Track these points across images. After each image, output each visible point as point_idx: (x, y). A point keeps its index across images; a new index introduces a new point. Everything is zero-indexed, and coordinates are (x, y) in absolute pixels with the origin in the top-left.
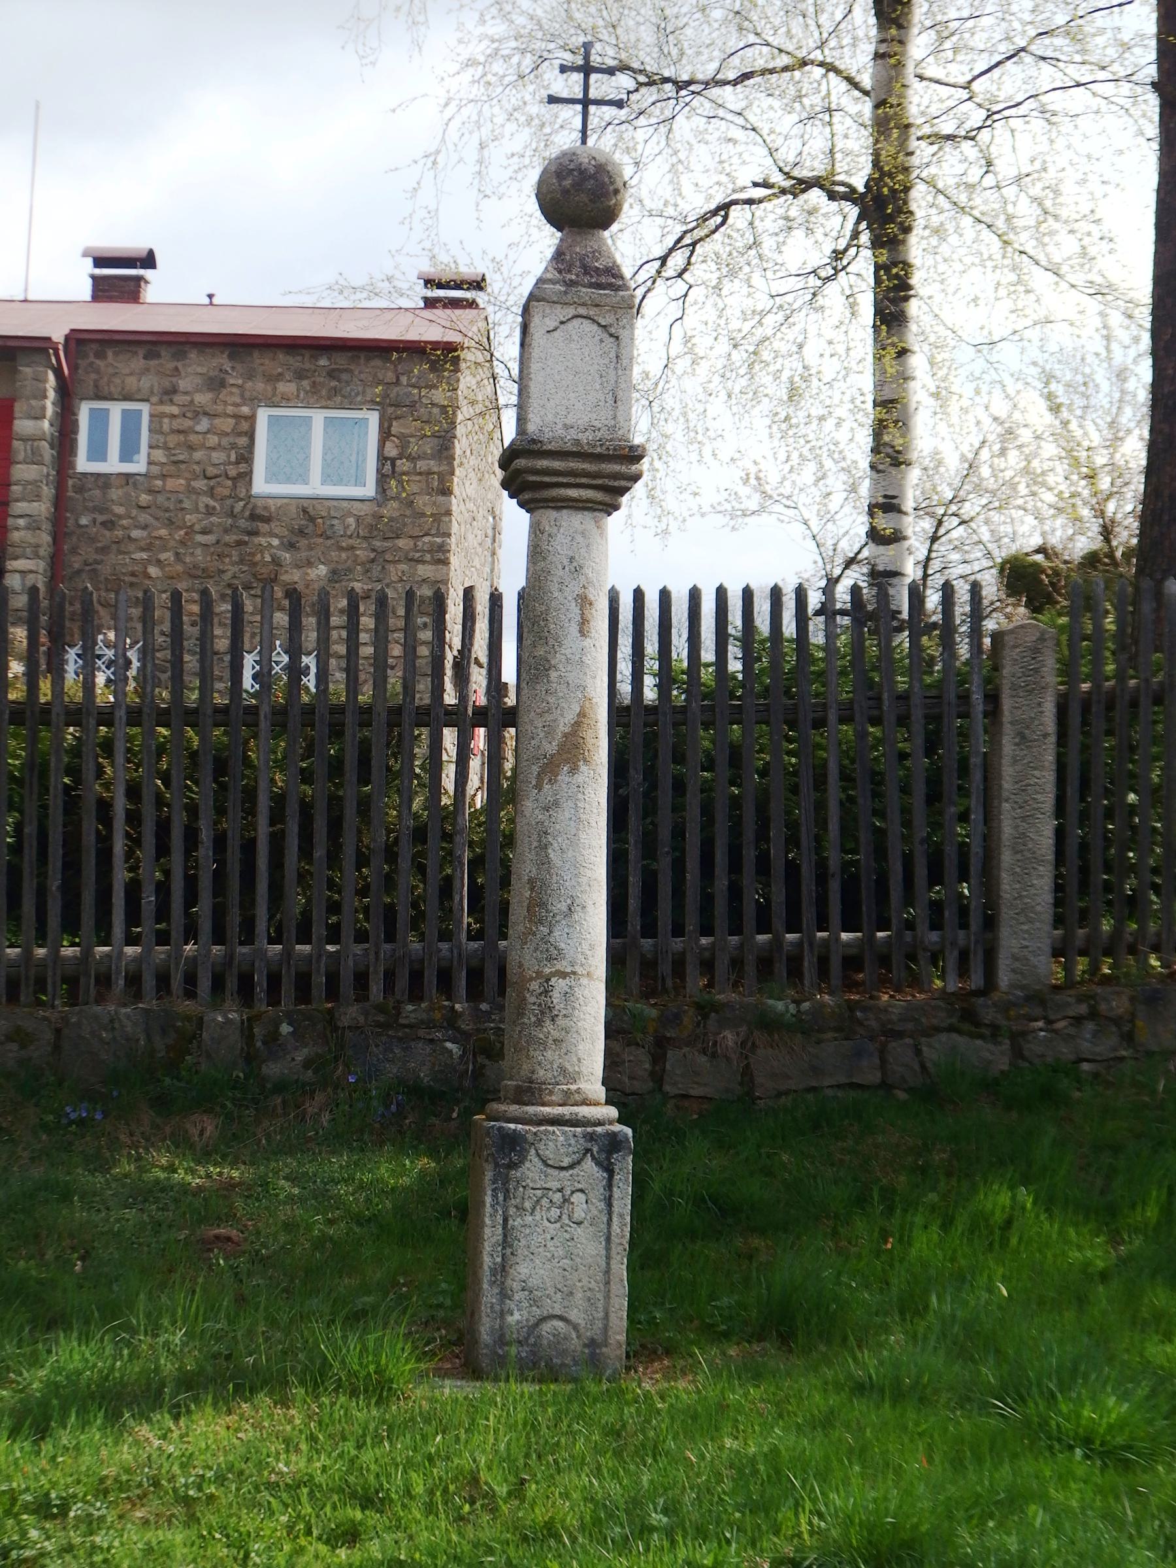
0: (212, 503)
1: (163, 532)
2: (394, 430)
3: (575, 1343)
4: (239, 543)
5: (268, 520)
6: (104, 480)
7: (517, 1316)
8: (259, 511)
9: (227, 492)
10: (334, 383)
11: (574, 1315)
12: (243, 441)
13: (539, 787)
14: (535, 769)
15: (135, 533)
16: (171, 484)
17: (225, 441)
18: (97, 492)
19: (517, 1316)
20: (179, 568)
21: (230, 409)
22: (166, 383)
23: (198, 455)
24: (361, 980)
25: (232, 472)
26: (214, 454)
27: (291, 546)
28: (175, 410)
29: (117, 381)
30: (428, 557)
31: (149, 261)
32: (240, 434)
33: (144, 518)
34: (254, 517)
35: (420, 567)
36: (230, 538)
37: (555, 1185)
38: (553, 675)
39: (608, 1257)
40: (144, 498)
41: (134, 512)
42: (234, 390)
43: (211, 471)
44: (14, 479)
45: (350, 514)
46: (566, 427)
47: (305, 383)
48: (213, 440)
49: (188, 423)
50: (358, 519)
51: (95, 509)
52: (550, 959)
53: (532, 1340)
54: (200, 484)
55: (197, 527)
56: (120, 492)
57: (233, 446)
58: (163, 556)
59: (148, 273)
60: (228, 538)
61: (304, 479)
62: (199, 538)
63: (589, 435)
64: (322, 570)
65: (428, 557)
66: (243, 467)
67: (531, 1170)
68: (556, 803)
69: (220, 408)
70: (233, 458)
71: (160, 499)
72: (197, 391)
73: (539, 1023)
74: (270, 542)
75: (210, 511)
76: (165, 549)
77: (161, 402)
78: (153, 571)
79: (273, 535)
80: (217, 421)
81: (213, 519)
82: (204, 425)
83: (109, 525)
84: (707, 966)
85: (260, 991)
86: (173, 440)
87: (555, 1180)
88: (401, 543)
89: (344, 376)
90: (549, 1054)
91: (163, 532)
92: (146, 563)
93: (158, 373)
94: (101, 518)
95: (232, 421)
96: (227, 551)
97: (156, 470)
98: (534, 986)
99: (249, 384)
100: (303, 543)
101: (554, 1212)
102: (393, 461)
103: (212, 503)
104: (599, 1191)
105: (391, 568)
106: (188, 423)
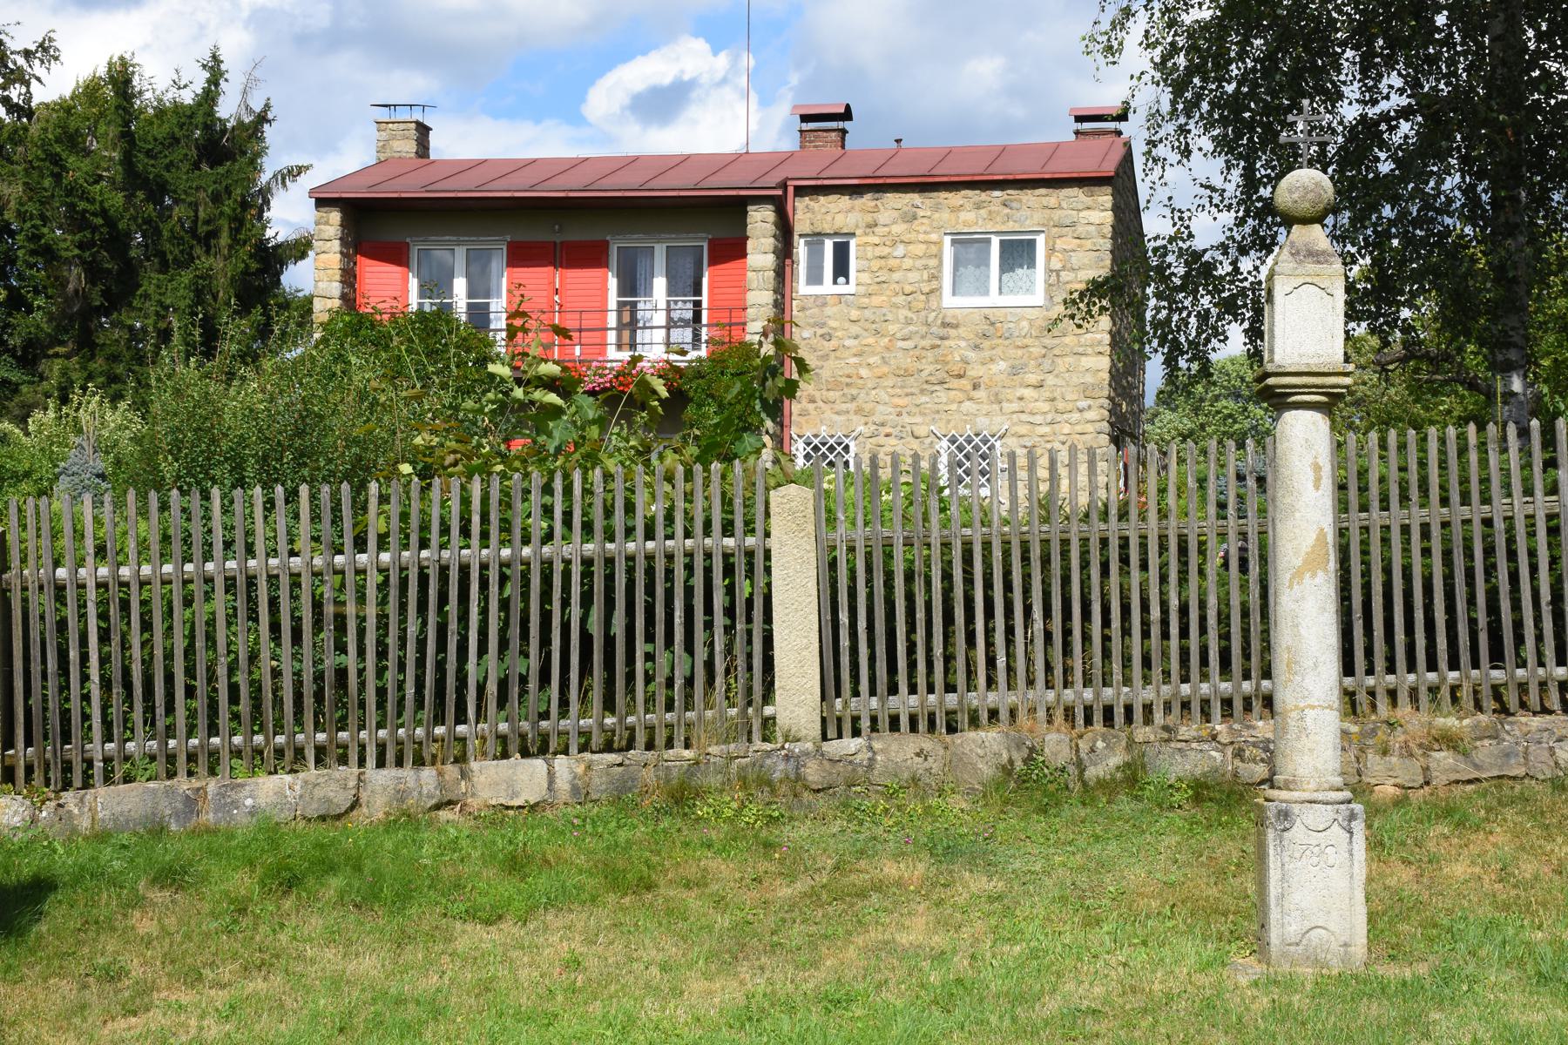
0: (910, 315)
1: (871, 340)
2: (1058, 247)
3: (1334, 946)
4: (934, 347)
5: (956, 326)
6: (822, 301)
7: (1294, 927)
8: (948, 320)
9: (921, 306)
10: (1007, 211)
11: (1332, 927)
12: (933, 262)
13: (1291, 587)
14: (1288, 576)
15: (848, 343)
16: (876, 301)
17: (919, 263)
18: (816, 310)
19: (1294, 927)
20: (885, 369)
21: (921, 237)
22: (869, 218)
23: (896, 276)
24: (1148, 709)
25: (926, 290)
26: (910, 275)
27: (977, 347)
28: (876, 240)
29: (829, 218)
30: (1090, 350)
31: (847, 115)
32: (930, 256)
33: (855, 329)
34: (945, 325)
35: (1083, 359)
36: (926, 343)
37: (1314, 842)
38: (1297, 515)
39: (1352, 888)
40: (854, 314)
41: (847, 325)
42: (925, 221)
43: (908, 289)
44: (749, 303)
45: (1023, 318)
46: (1300, 356)
47: (983, 212)
48: (908, 263)
49: (886, 250)
50: (1031, 321)
51: (816, 325)
52: (1304, 697)
53: (1304, 942)
54: (901, 299)
55: (899, 335)
56: (835, 309)
57: (926, 267)
58: (871, 360)
59: (847, 125)
60: (924, 343)
61: (986, 293)
62: (901, 344)
63: (1316, 360)
64: (1003, 365)
65: (1090, 350)
66: (934, 284)
67: (1297, 833)
68: (1303, 598)
69: (913, 236)
70: (925, 277)
71: (867, 313)
72: (894, 223)
73: (1298, 738)
74: (958, 348)
75: (908, 322)
76: (873, 354)
77: (866, 234)
78: (864, 372)
79: (959, 338)
80: (911, 247)
81: (911, 328)
82: (900, 250)
83: (827, 337)
84: (1392, 694)
85: (1080, 720)
86: (875, 264)
87: (1315, 838)
88: (1067, 340)
89: (1014, 205)
90: (1306, 758)
91: (871, 340)
92: (857, 366)
93: (862, 210)
94: (820, 332)
95: (924, 247)
96: (924, 353)
97: (862, 289)
98: (1294, 714)
99: (937, 215)
100: (986, 344)
101: (1315, 860)
102: (1057, 272)
103: (910, 315)
104: (1345, 846)
105: (1059, 361)
106: (886, 250)
